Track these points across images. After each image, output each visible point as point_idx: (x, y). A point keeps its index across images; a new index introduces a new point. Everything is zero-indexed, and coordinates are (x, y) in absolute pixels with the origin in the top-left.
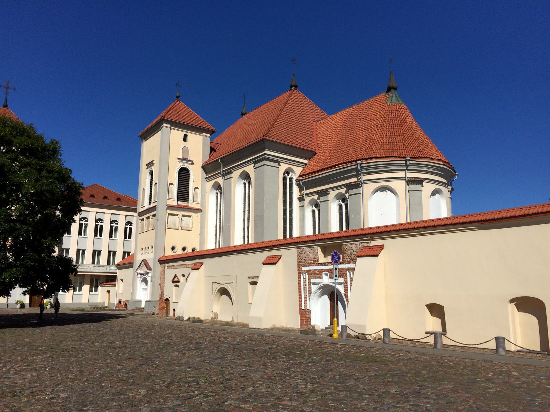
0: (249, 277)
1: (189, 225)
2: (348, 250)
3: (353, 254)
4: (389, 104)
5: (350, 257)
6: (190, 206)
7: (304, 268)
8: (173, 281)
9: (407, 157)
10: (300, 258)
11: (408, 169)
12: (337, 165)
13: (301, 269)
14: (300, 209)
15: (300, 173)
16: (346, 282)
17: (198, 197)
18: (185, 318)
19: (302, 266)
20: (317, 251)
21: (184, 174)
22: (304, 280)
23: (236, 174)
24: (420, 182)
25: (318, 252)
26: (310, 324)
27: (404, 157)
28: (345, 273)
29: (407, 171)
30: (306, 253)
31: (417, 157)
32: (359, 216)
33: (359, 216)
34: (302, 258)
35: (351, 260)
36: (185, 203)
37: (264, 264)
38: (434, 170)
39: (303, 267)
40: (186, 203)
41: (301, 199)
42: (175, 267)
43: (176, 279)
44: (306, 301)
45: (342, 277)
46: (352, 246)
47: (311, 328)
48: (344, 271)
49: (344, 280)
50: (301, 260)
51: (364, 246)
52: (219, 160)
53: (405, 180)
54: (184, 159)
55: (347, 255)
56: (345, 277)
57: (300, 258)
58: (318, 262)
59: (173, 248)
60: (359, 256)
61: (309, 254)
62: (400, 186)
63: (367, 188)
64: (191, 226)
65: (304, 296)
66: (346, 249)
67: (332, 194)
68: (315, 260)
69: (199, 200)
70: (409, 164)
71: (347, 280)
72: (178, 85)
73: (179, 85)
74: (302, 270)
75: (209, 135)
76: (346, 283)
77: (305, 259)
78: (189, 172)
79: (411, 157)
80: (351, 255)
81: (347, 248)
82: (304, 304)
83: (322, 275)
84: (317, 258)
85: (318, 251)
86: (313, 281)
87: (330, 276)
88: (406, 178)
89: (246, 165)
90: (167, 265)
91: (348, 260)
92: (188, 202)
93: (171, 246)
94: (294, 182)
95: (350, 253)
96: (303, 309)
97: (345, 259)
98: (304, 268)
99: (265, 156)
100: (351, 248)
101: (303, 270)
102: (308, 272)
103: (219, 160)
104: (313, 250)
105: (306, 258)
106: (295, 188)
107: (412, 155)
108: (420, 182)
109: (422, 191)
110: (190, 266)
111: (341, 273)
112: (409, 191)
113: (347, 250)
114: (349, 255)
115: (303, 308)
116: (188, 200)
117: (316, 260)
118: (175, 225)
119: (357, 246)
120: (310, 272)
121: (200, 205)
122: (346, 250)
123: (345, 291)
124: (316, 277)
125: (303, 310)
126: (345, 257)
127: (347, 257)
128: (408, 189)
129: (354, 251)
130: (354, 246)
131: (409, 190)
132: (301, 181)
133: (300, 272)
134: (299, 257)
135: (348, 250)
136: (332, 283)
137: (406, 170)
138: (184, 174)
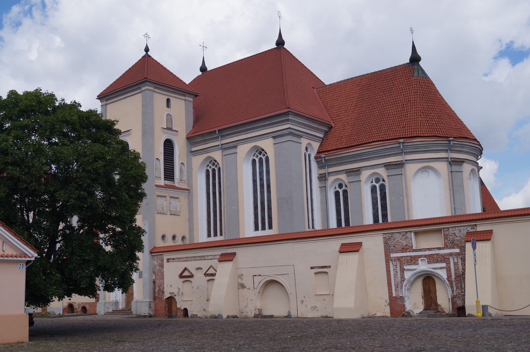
0: (312, 268)
1: (176, 208)
2: (450, 235)
3: (455, 240)
4: (417, 78)
5: (453, 242)
6: (177, 186)
7: (393, 255)
8: (181, 276)
9: (450, 137)
10: (388, 245)
11: (451, 149)
12: (369, 143)
13: (390, 256)
14: (320, 189)
15: (318, 149)
16: (448, 267)
17: (183, 174)
18: (225, 316)
19: (390, 253)
20: (410, 237)
21: (169, 145)
22: (395, 267)
23: (243, 149)
24: (461, 162)
25: (411, 239)
26: (404, 311)
27: (447, 137)
28: (447, 258)
29: (450, 151)
30: (396, 240)
31: (457, 138)
32: (401, 198)
33: (401, 198)
34: (391, 245)
35: (453, 245)
36: (171, 183)
37: (340, 252)
38: (471, 150)
39: (393, 253)
40: (172, 182)
41: (322, 178)
42: (181, 260)
43: (186, 273)
44: (397, 289)
45: (444, 262)
46: (454, 232)
47: (406, 314)
48: (446, 256)
49: (447, 265)
50: (390, 247)
51: (469, 231)
52: (217, 131)
53: (448, 160)
54: (169, 129)
55: (449, 240)
56: (447, 262)
57: (388, 245)
58: (412, 248)
59: (163, 237)
60: (477, 241)
61: (400, 241)
62: (443, 167)
63: (410, 169)
64: (178, 210)
65: (395, 283)
66: (447, 234)
67: (365, 174)
68: (408, 246)
69: (185, 178)
70: (453, 144)
71: (450, 265)
72: (147, 37)
73: (148, 36)
74: (391, 257)
75: (191, 100)
76: (448, 268)
77: (394, 246)
78: (171, 143)
79: (455, 138)
80: (454, 240)
81: (448, 234)
82: (395, 291)
83: (418, 261)
84: (411, 244)
85: (411, 237)
86: (406, 267)
87: (428, 262)
88: (449, 158)
89: (259, 139)
90: (166, 256)
91: (450, 246)
92: (174, 181)
93: (162, 235)
94: (312, 158)
95: (453, 239)
96: (393, 296)
97: (446, 244)
98: (393, 255)
99: (290, 130)
100: (454, 233)
101: (392, 257)
102: (399, 259)
103: (217, 131)
104: (405, 236)
105: (395, 244)
106: (314, 165)
107: (447, 134)
108: (461, 162)
109: (463, 172)
110: (216, 257)
111: (442, 258)
112: (451, 172)
113: (449, 236)
114: (451, 241)
115: (394, 295)
116: (174, 179)
117: (409, 247)
118: (163, 209)
119: (461, 231)
120: (402, 258)
121: (187, 184)
122: (447, 236)
123: (448, 275)
124: (410, 264)
125: (393, 298)
126: (446, 242)
127: (449, 242)
128: (450, 170)
129: (457, 237)
130: (457, 232)
131: (452, 171)
132: (323, 158)
133: (388, 259)
134: (386, 243)
135: (450, 235)
136: (431, 268)
137: (449, 151)
138: (169, 145)
